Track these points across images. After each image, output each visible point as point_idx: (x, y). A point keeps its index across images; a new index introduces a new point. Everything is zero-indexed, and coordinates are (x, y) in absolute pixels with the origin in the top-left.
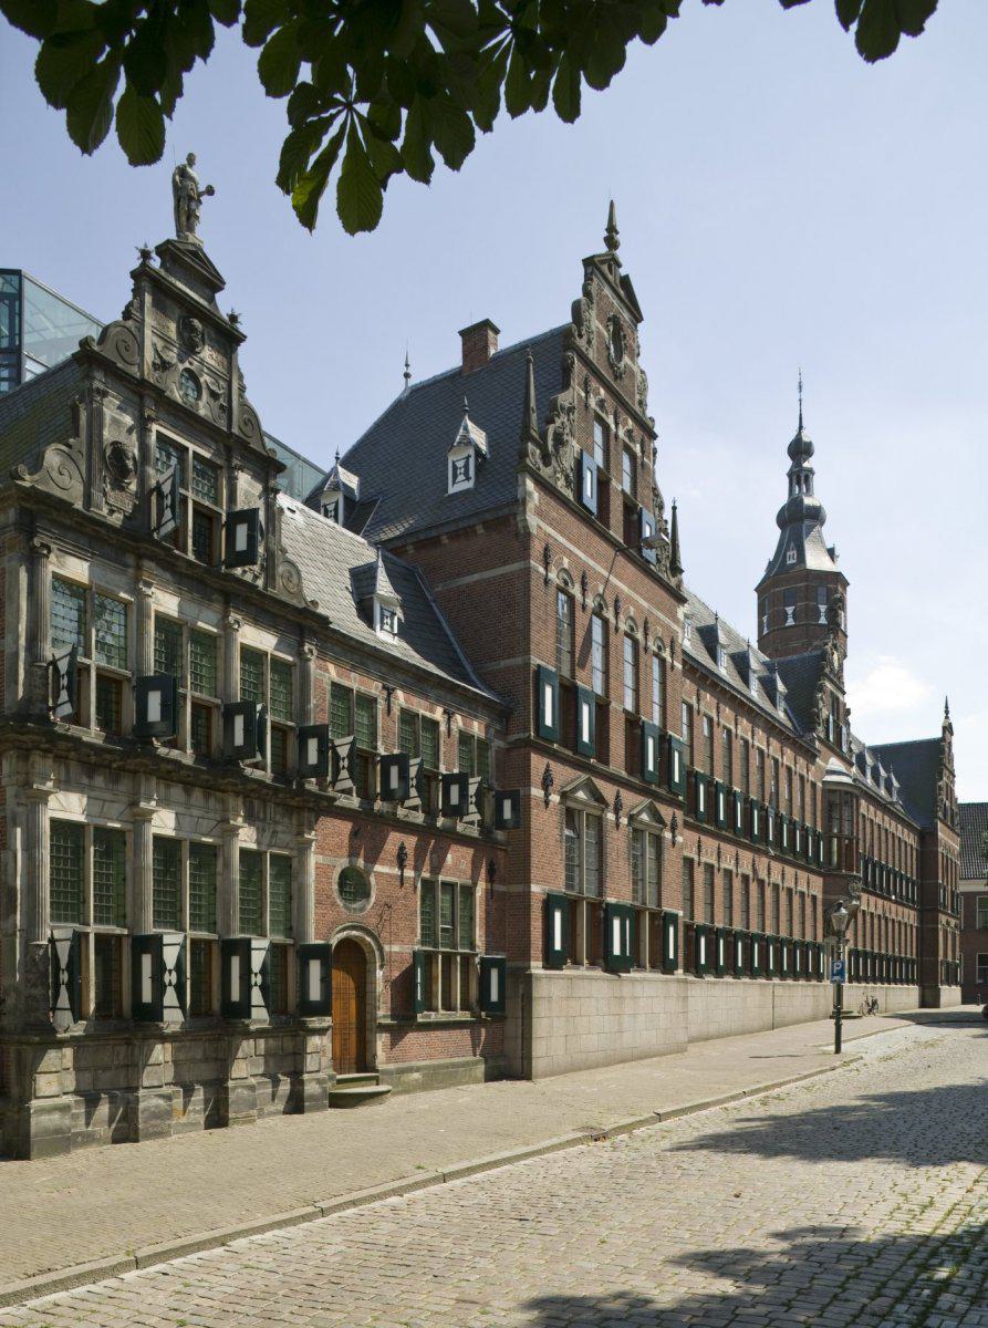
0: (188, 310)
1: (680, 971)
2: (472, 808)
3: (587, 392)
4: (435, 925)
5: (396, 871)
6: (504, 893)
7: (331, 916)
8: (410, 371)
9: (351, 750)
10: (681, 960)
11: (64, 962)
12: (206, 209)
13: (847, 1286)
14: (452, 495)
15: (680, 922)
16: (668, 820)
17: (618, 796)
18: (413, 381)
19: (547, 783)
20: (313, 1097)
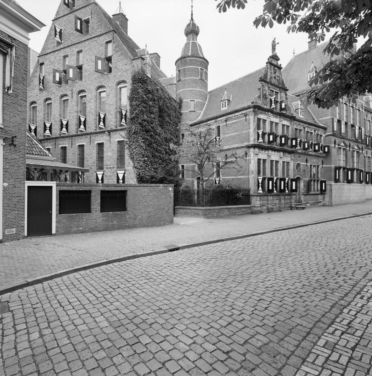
0: (275, 66)
1: (364, 183)
2: (298, 146)
3: (343, 54)
4: (185, 163)
5: (306, 164)
6: (325, 167)
7: (295, 173)
8: (295, 52)
9: (262, 133)
10: (364, 180)
11: (260, 182)
12: (277, 47)
13: (357, 316)
14: (286, 67)
15: (364, 171)
16: (348, 145)
17: (350, 144)
18: (295, 54)
19: (335, 143)
20: (294, 207)
